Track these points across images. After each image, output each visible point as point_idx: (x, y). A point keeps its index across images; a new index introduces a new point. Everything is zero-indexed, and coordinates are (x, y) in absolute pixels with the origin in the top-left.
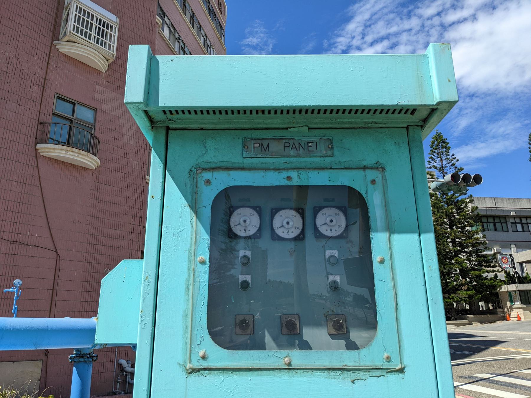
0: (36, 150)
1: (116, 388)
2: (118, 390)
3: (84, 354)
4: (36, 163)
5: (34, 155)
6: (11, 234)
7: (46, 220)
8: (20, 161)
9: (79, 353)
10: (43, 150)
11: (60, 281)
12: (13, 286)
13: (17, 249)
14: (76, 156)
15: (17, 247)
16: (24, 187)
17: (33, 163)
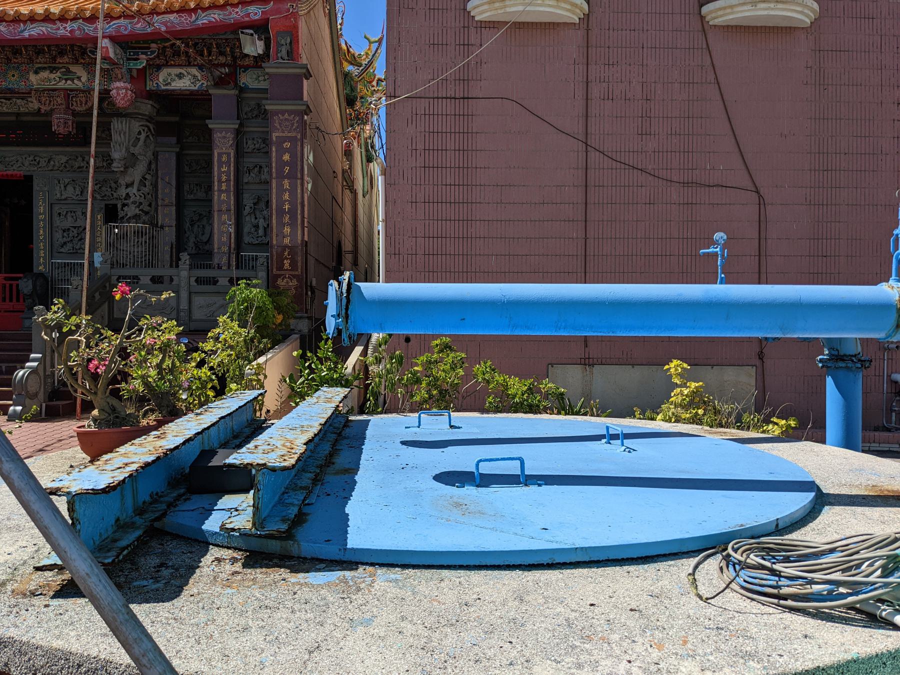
0: (702, 18)
1: (889, 420)
2: (893, 425)
3: (845, 355)
4: (704, 42)
5: (700, 28)
6: (682, 171)
7: (733, 140)
8: (679, 46)
9: (836, 353)
10: (713, 15)
11: (769, 241)
12: (715, 243)
13: (694, 195)
14: (772, 9)
15: (694, 191)
16: (691, 90)
17: (700, 42)
